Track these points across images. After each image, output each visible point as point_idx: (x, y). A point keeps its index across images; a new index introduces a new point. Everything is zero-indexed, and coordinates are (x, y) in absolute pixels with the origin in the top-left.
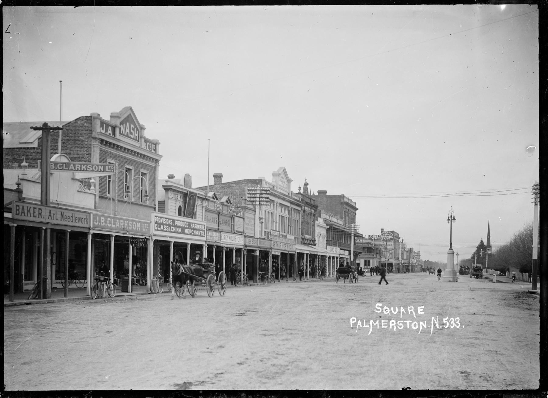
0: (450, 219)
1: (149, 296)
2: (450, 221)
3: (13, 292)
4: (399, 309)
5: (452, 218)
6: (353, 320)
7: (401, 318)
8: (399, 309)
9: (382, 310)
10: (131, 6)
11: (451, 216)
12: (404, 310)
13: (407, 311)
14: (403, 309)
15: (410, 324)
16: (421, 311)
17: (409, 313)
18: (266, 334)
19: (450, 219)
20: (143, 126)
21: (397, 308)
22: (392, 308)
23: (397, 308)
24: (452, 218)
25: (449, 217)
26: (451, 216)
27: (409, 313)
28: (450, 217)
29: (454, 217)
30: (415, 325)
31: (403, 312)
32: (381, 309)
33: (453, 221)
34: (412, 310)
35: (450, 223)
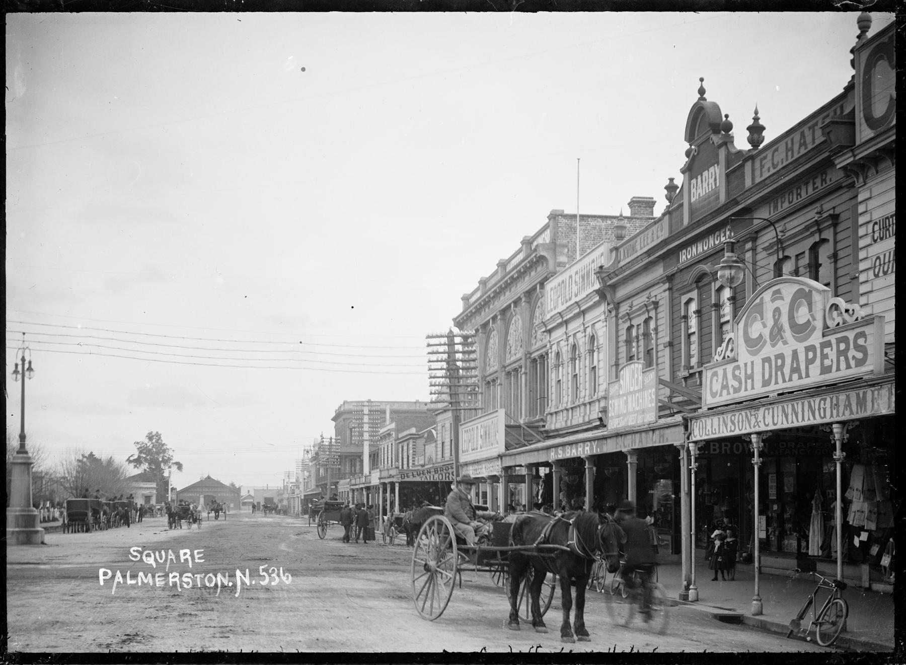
0: (20, 368)
1: (145, 545)
2: (19, 376)
3: (466, 546)
4: (167, 553)
5: (26, 366)
6: (105, 574)
7: (129, 572)
8: (167, 553)
9: (141, 557)
10: (78, 12)
11: (23, 360)
12: (173, 557)
13: (178, 557)
14: (172, 554)
15: (202, 580)
16: (199, 558)
17: (182, 561)
18: (403, 596)
19: (20, 368)
20: (501, 262)
21: (163, 552)
22: (157, 553)
23: (163, 552)
24: (26, 366)
25: (16, 365)
26: (23, 360)
27: (182, 561)
28: (20, 363)
29: (30, 363)
30: (210, 580)
31: (172, 559)
32: (139, 556)
33: (27, 373)
34: (188, 556)
35: (20, 382)
